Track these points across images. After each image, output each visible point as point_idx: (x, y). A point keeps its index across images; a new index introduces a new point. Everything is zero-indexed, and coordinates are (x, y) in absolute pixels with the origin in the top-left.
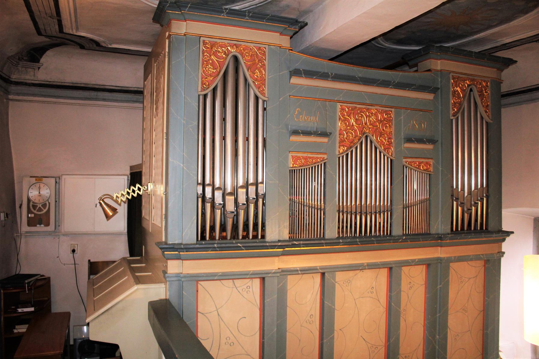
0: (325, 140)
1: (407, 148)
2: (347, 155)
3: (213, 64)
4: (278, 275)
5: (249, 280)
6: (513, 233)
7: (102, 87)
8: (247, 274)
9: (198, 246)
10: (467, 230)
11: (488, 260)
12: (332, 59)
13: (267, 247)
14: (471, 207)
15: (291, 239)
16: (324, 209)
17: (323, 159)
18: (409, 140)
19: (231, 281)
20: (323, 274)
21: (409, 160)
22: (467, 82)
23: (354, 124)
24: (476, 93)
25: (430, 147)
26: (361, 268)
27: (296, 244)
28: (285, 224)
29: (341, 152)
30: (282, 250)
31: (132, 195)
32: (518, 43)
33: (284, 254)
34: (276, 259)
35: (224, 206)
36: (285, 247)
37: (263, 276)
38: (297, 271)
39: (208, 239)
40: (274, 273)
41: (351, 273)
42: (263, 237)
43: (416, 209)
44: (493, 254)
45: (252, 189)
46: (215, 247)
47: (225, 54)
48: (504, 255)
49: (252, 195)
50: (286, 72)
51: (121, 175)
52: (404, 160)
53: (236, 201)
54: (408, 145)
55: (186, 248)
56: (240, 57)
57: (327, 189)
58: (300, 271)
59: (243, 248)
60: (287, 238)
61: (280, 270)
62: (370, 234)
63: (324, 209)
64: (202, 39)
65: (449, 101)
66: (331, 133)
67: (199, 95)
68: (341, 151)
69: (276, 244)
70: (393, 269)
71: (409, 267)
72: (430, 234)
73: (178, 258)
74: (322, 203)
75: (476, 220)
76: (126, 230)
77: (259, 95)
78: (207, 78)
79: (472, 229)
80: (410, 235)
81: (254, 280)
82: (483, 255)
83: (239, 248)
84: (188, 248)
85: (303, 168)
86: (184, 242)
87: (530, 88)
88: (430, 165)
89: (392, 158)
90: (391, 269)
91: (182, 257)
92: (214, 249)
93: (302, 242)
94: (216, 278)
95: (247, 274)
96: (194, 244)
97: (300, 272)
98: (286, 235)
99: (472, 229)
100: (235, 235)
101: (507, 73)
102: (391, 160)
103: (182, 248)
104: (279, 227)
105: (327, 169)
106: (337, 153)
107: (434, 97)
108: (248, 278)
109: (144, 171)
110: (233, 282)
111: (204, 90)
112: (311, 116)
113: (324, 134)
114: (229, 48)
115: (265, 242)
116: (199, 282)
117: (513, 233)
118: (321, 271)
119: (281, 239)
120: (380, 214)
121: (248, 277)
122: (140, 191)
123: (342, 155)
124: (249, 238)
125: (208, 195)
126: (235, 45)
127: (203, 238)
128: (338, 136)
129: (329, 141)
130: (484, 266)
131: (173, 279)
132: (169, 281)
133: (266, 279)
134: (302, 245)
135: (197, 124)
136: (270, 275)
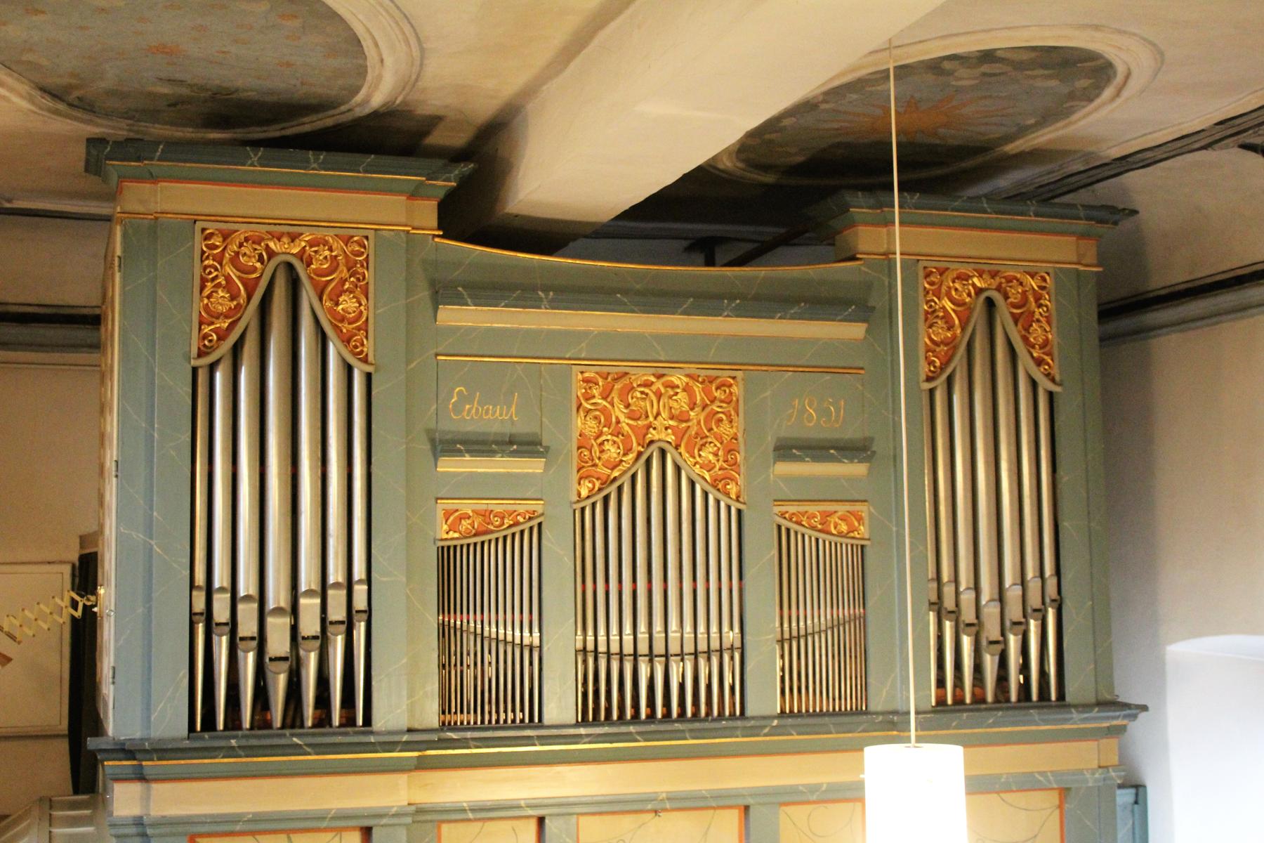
1: (788, 479)
2: (606, 500)
4: (409, 820)
5: (330, 835)
10: (1019, 700)
11: (1068, 789)
13: (372, 747)
14: (1003, 634)
15: (444, 726)
18: (786, 450)
19: (283, 837)
20: (541, 821)
21: (792, 509)
22: (976, 280)
23: (622, 418)
24: (1004, 313)
25: (857, 469)
28: (429, 688)
30: (416, 754)
32: (1158, 154)
33: (422, 765)
34: (402, 779)
36: (425, 748)
38: (464, 810)
39: (221, 726)
41: (627, 822)
43: (820, 643)
44: (1081, 772)
45: (337, 600)
46: (233, 748)
47: (261, 259)
50: (424, 294)
51: (29, 563)
52: (777, 509)
53: (294, 629)
54: (784, 468)
58: (473, 810)
59: (309, 750)
60: (434, 722)
61: (413, 808)
65: (917, 340)
67: (195, 370)
68: (584, 493)
69: (396, 738)
70: (751, 809)
72: (867, 713)
75: (1025, 668)
77: (352, 360)
79: (1053, 697)
80: (814, 715)
82: (1042, 773)
83: (296, 749)
85: (479, 539)
87: (1240, 272)
88: (860, 519)
91: (146, 772)
92: (230, 752)
93: (469, 735)
98: (430, 716)
99: (1053, 697)
100: (323, 720)
104: (410, 696)
105: (544, 542)
107: (867, 331)
108: (326, 830)
109: (1095, 324)
111: (206, 354)
112: (495, 406)
115: (372, 733)
119: (417, 726)
120: (709, 659)
122: (76, 610)
124: (331, 726)
125: (221, 612)
127: (209, 723)
128: (575, 453)
130: (1060, 807)
133: (374, 831)
134: (472, 743)
135: (189, 440)
136: (384, 821)
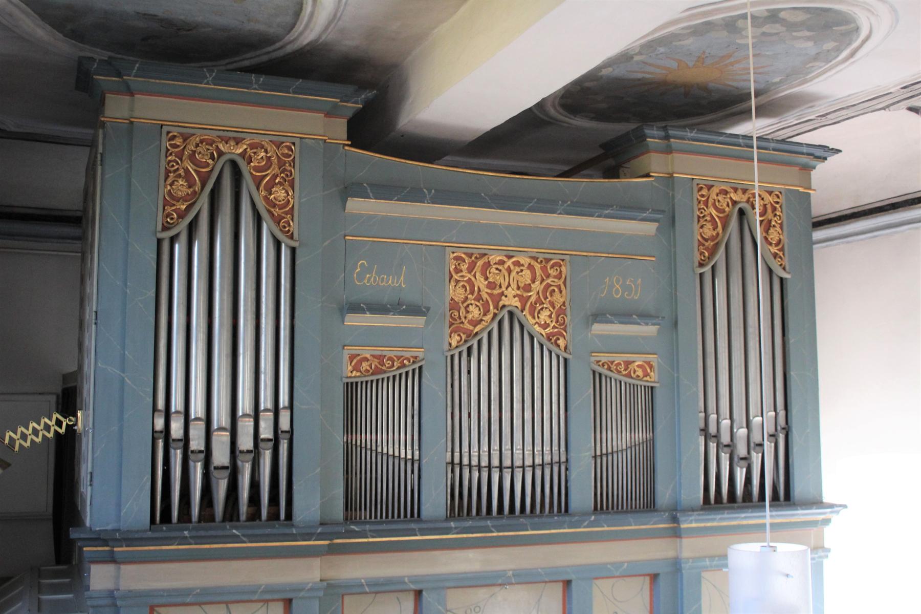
0: (417, 322)
2: (469, 350)
3: (187, 176)
6: (845, 506)
7: (8, 210)
8: (254, 592)
9: (150, 534)
12: (897, 21)
14: (749, 452)
16: (419, 460)
17: (415, 359)
26: (500, 581)
27: (354, 531)
29: (454, 344)
30: (326, 542)
31: (16, 433)
35: (208, 452)
37: (289, 596)
40: (311, 589)
42: (289, 516)
48: (830, 555)
49: (266, 432)
55: (125, 539)
56: (242, 164)
57: (423, 421)
59: (244, 539)
62: (541, 512)
63: (419, 460)
64: (165, 129)
66: (428, 309)
71: (611, 581)
73: (112, 559)
74: (416, 447)
76: (50, 510)
77: (281, 236)
78: (174, 205)
81: (270, 604)
84: (130, 539)
86: (124, 526)
87: (893, 201)
89: (566, 356)
90: (567, 583)
94: (188, 600)
95: (254, 592)
96: (145, 531)
97: (367, 590)
100: (255, 516)
101: (821, 173)
102: (566, 360)
103: (116, 540)
105: (424, 380)
106: (446, 347)
110: (228, 608)
112: (388, 276)
113: (415, 310)
114: (221, 146)
116: (157, 609)
117: (845, 506)
118: (413, 587)
121: (256, 597)
122: (61, 427)
123: (460, 349)
124: (260, 520)
126: (234, 138)
129: (427, 323)
131: (101, 602)
132: (93, 607)
135: (154, 295)
